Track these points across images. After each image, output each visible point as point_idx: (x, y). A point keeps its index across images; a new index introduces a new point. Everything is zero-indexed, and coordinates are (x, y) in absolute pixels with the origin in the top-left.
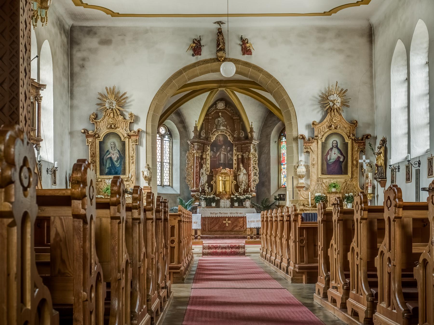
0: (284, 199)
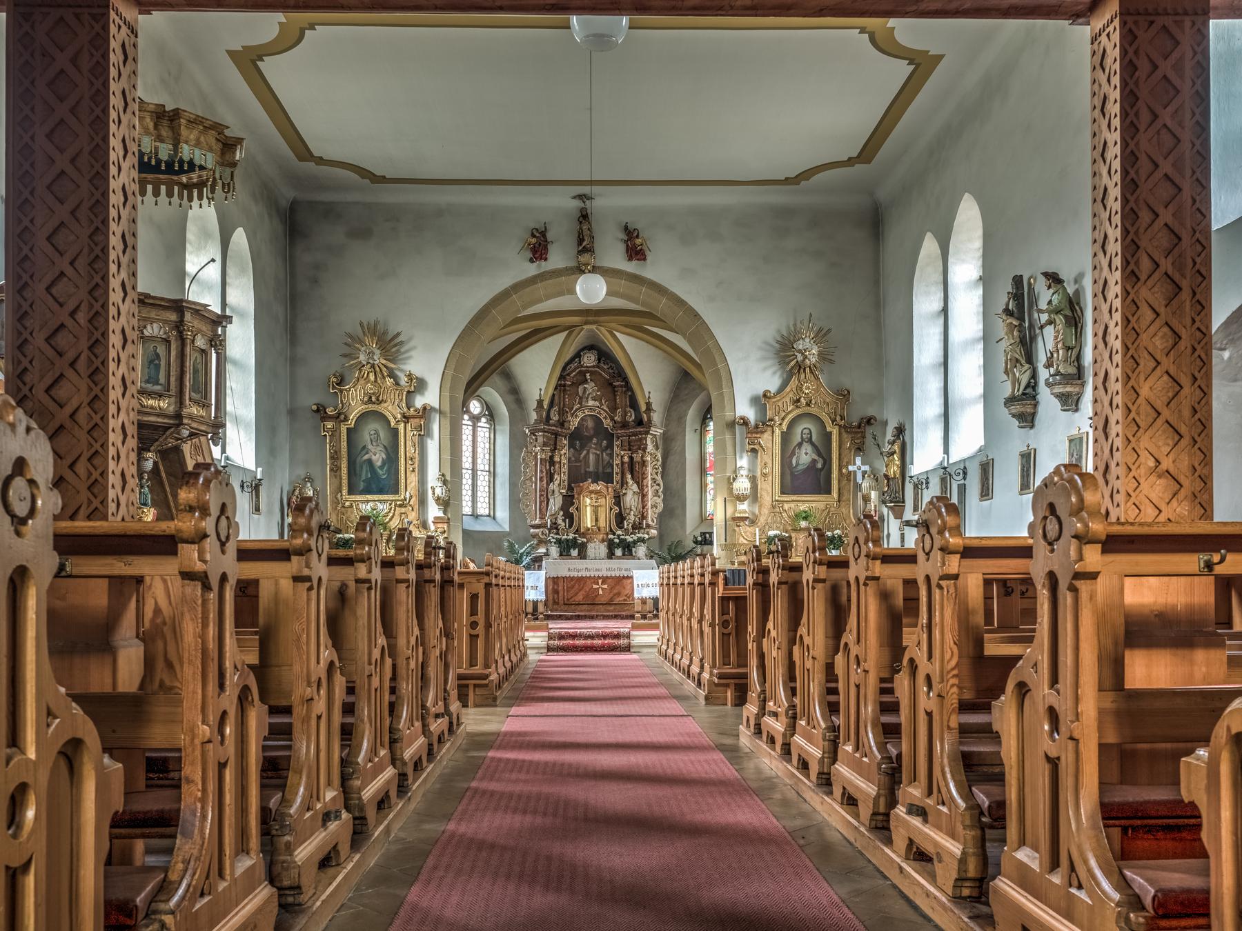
0: (711, 543)
